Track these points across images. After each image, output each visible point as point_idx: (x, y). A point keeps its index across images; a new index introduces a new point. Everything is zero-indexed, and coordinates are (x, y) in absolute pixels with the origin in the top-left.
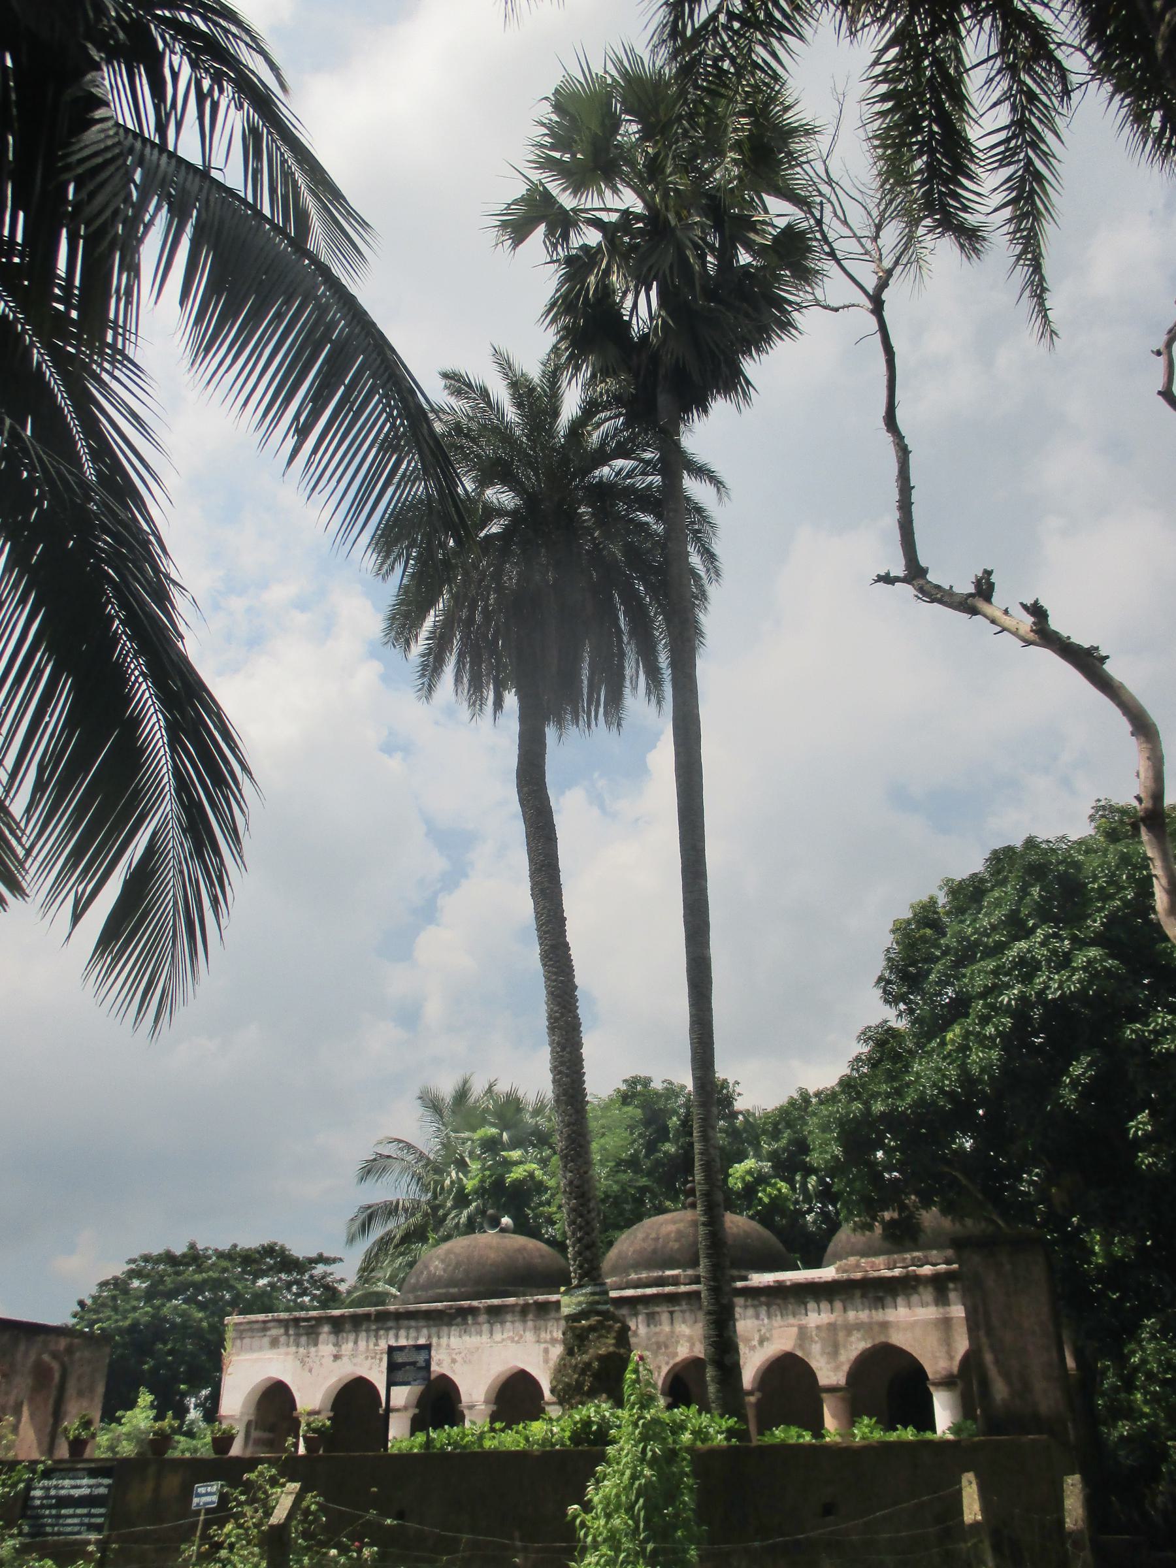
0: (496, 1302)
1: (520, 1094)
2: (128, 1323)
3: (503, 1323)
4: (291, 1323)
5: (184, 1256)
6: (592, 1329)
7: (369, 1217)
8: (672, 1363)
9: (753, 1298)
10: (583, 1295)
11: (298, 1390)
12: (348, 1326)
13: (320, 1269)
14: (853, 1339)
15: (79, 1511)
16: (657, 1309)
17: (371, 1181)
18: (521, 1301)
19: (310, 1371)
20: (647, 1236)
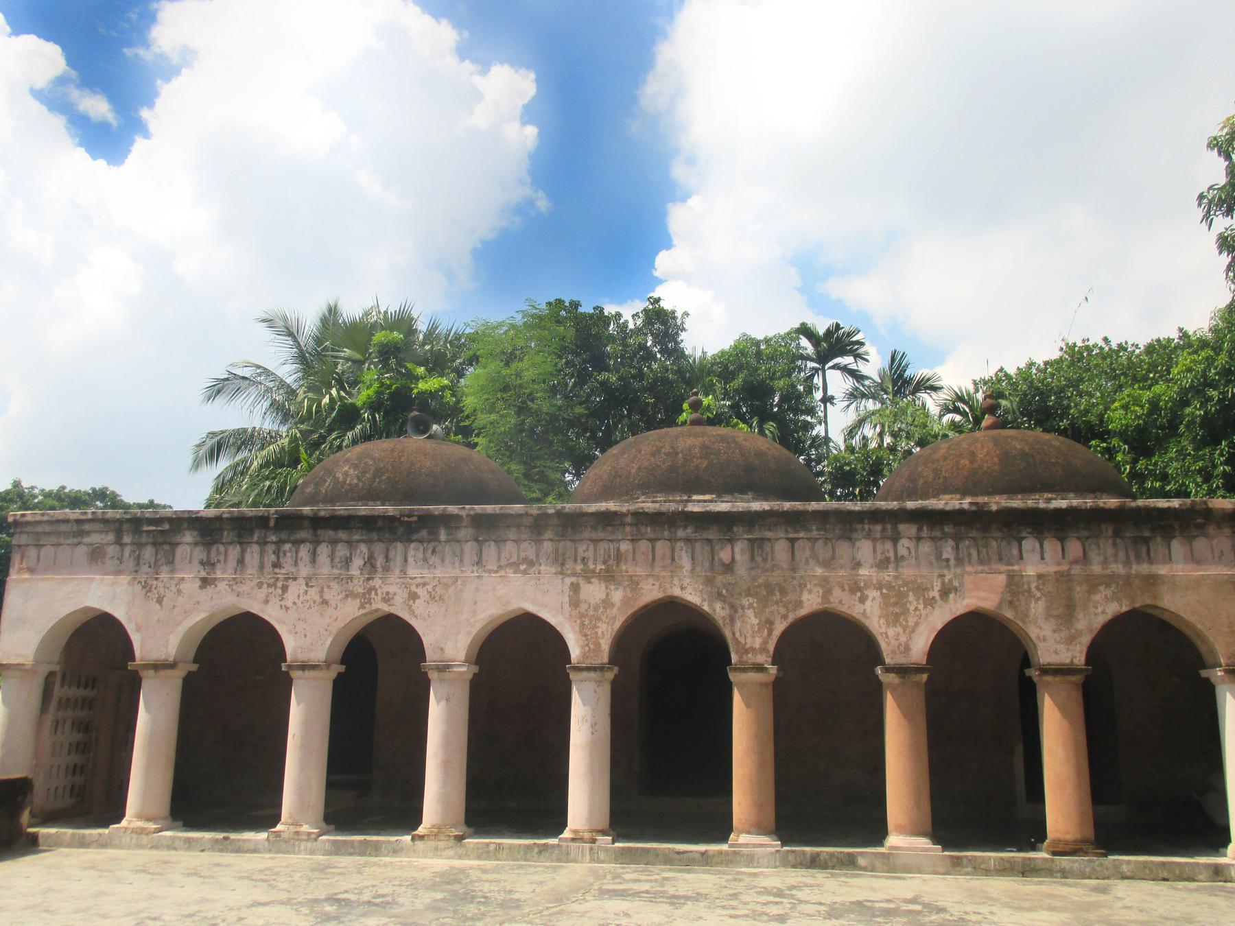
0: (489, 508)
1: (415, 314)
3: (500, 542)
7: (216, 447)
8: (792, 617)
9: (932, 527)
11: (138, 629)
12: (227, 536)
14: (1098, 597)
16: (769, 534)
17: (220, 400)
18: (534, 509)
19: (160, 601)
20: (658, 451)
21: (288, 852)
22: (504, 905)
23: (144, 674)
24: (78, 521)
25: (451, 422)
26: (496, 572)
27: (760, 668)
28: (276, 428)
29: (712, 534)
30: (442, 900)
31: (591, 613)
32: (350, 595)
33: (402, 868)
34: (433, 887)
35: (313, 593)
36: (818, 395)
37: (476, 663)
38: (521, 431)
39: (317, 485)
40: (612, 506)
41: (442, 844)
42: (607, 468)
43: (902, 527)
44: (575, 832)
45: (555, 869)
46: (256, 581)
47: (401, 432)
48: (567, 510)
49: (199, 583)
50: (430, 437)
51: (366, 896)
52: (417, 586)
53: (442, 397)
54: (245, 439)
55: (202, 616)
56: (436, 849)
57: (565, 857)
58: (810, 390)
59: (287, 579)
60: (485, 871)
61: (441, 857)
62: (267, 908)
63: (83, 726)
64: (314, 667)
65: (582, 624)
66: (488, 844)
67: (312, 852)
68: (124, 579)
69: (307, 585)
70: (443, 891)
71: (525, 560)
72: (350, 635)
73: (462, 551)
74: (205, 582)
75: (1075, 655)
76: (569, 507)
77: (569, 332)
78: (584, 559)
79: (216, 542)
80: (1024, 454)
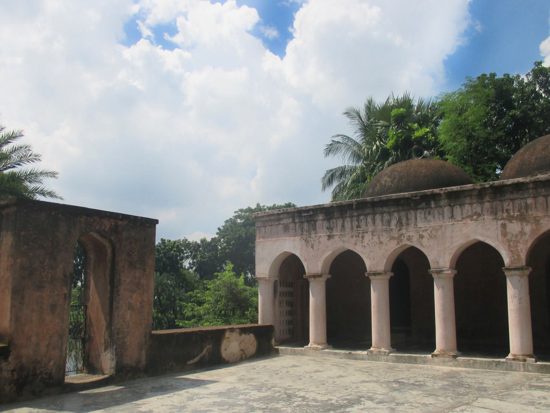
0: (455, 188)
2: (237, 236)
3: (462, 205)
4: (296, 215)
5: (255, 209)
11: (305, 260)
12: (336, 214)
17: (331, 155)
18: (478, 187)
19: (312, 247)
21: (376, 360)
22: (478, 389)
23: (310, 280)
24: (278, 214)
25: (434, 150)
26: (461, 221)
28: (354, 165)
30: (448, 385)
31: (514, 239)
32: (392, 238)
33: (428, 369)
34: (443, 379)
35: (375, 238)
37: (456, 269)
38: (471, 149)
40: (521, 180)
41: (447, 359)
42: (518, 161)
44: (514, 355)
45: (505, 374)
46: (350, 235)
47: (410, 157)
48: (496, 184)
49: (327, 238)
50: (424, 157)
51: (412, 381)
52: (423, 231)
53: (427, 138)
54: (343, 172)
55: (330, 253)
56: (444, 361)
57: (509, 368)
59: (363, 233)
60: (468, 373)
61: (446, 365)
62: (368, 384)
63: (290, 304)
64: (379, 274)
65: (509, 245)
66: (469, 360)
67: (387, 361)
68: (298, 238)
69: (372, 235)
70: (447, 381)
71: (476, 213)
72: (394, 258)
73: (443, 212)
74: (330, 237)
76: (496, 183)
78: (507, 210)
79: (332, 218)
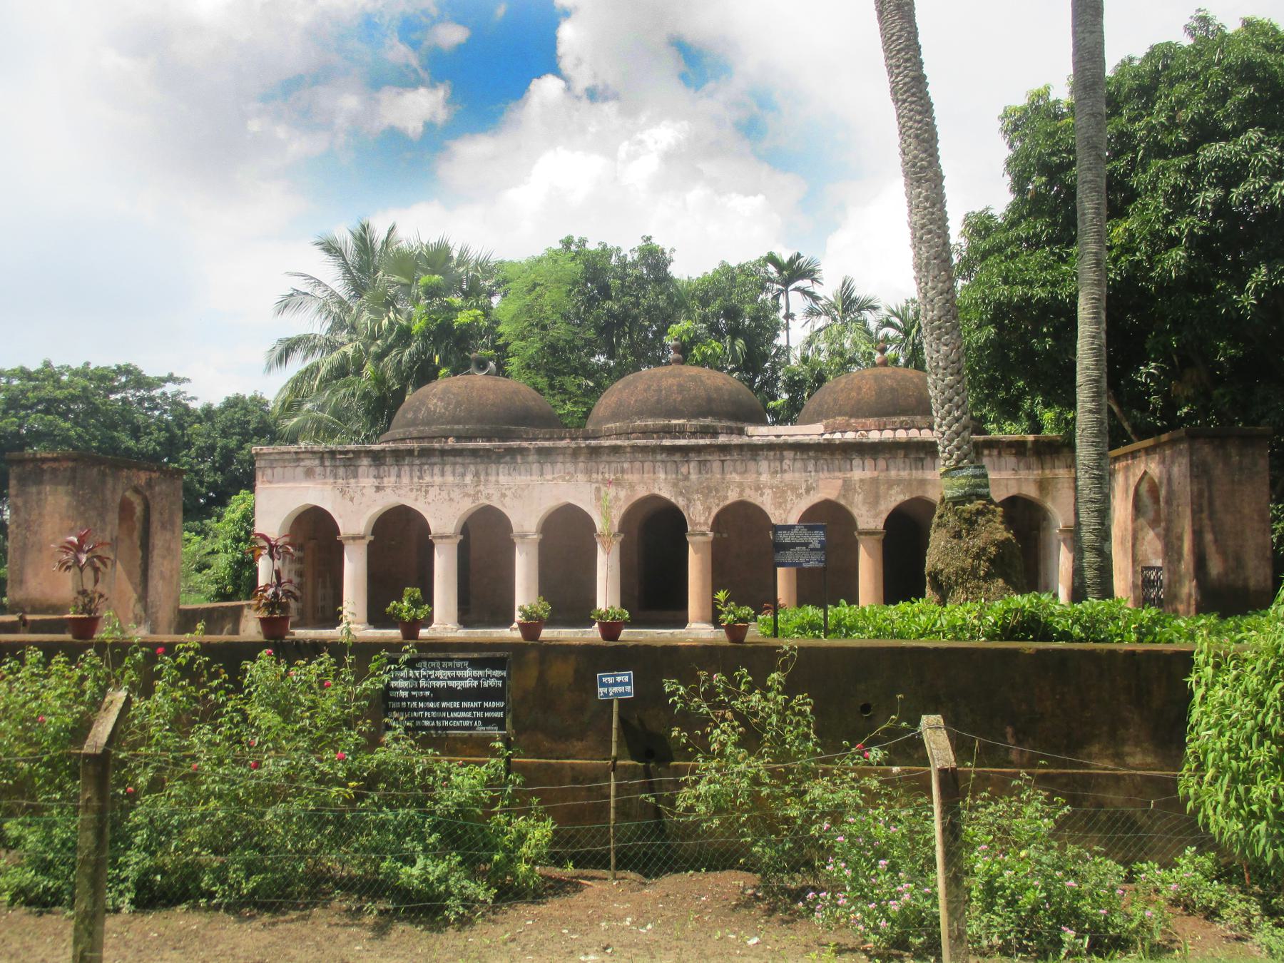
1: (451, 244)
3: (553, 463)
6: (979, 513)
7: (288, 349)
8: (722, 505)
9: (802, 452)
10: (964, 477)
13: (170, 388)
14: (893, 492)
15: (466, 705)
16: (710, 458)
17: (288, 314)
18: (573, 444)
19: (352, 500)
20: (649, 387)
27: (704, 534)
29: (677, 457)
35: (444, 494)
36: (783, 312)
39: (415, 412)
43: (786, 453)
58: (777, 308)
64: (448, 537)
74: (378, 489)
75: (879, 524)
77: (577, 268)
80: (893, 390)
